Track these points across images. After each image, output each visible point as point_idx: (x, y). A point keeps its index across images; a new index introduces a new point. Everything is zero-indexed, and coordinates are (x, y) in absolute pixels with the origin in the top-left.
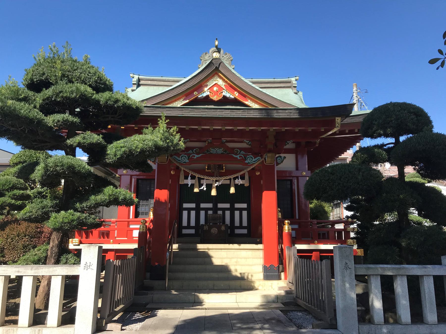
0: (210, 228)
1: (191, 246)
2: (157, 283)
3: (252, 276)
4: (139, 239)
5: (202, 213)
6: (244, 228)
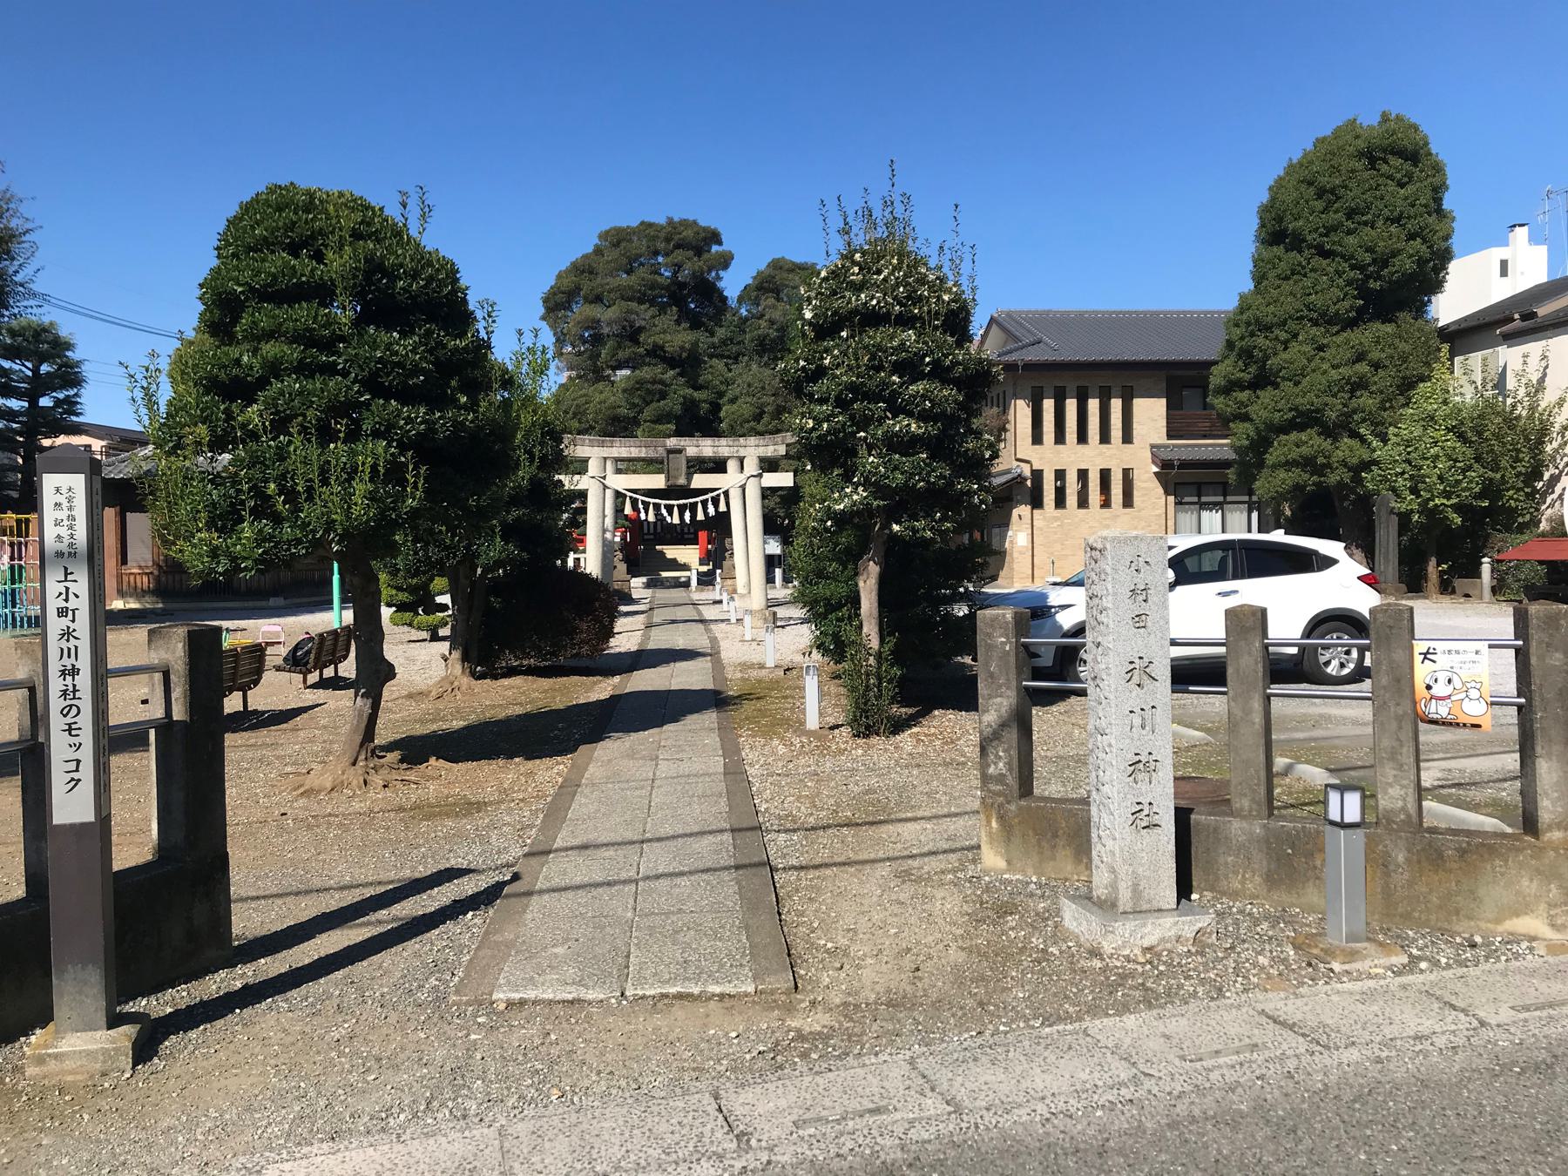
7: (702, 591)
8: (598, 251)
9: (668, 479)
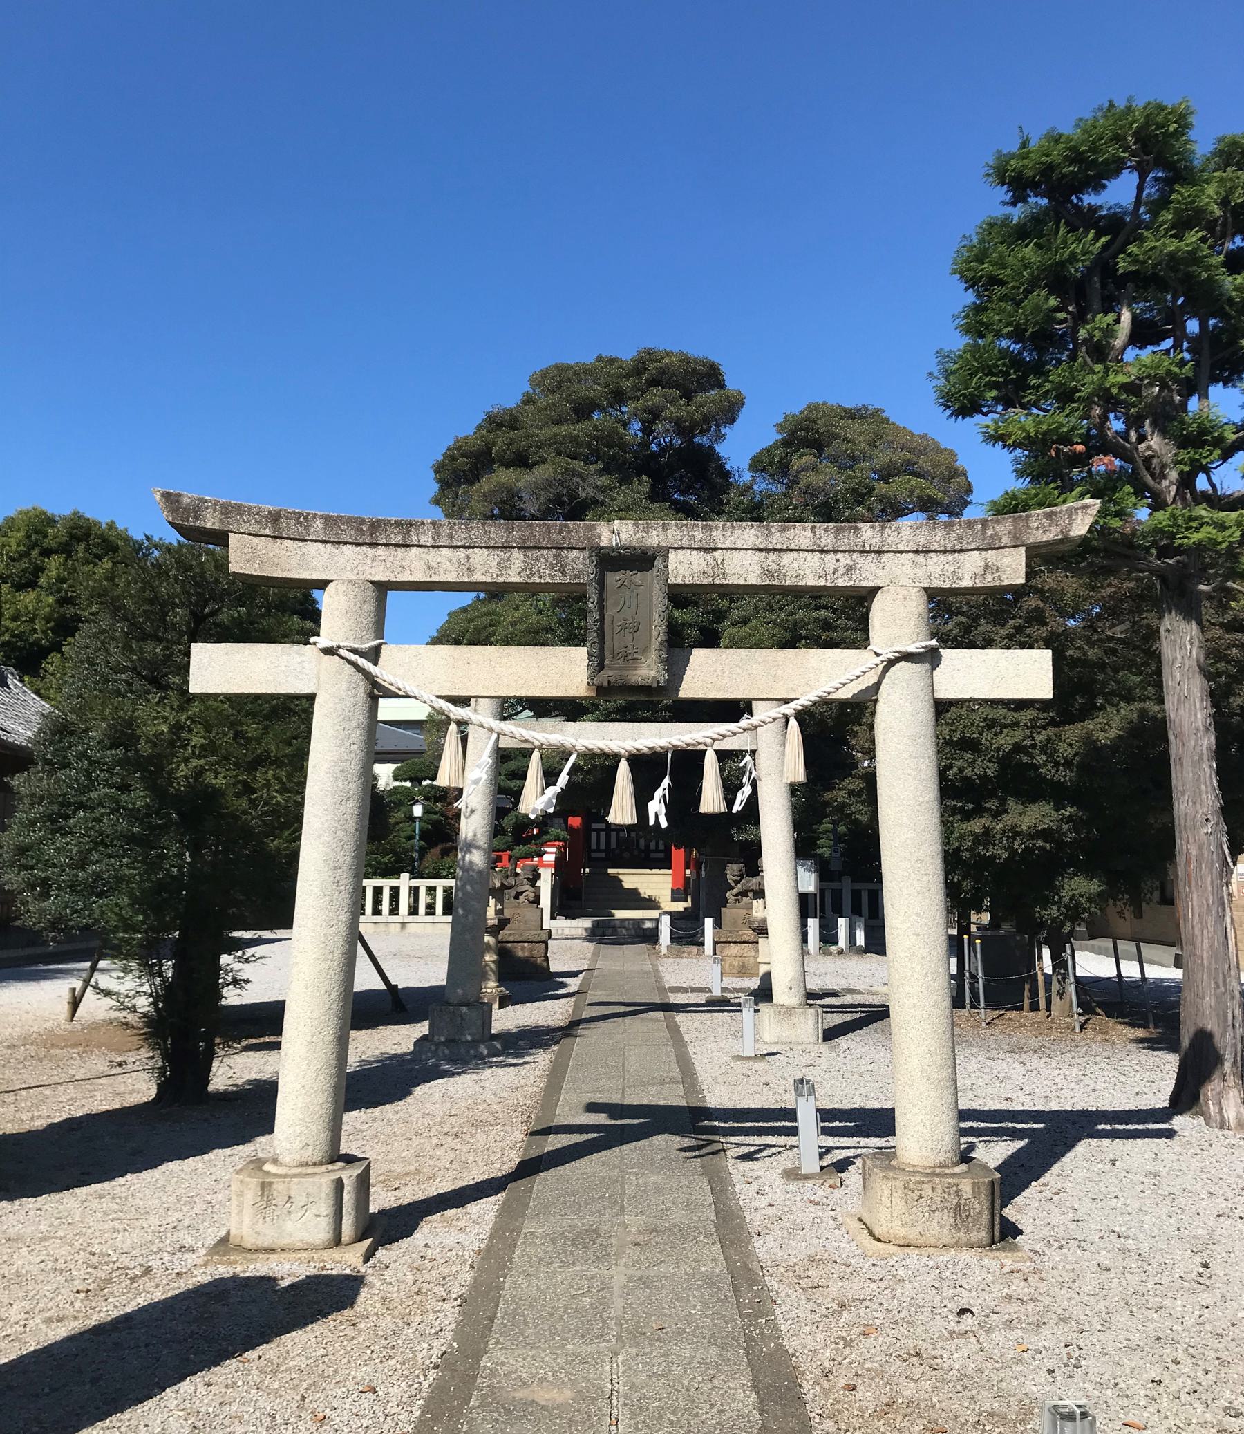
7: (679, 955)
8: (528, 401)
9: (598, 663)
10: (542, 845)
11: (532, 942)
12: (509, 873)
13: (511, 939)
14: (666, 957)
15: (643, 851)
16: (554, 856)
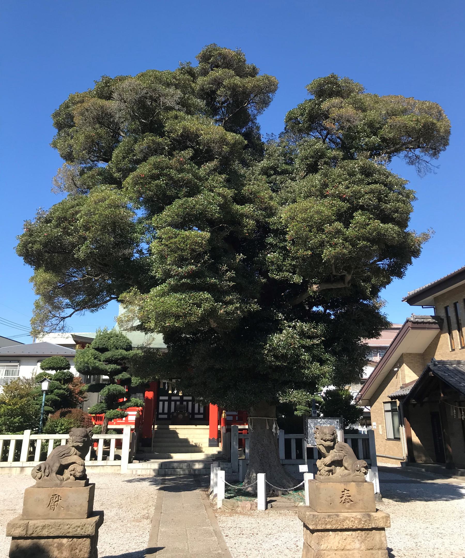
0: (178, 414)
1: (165, 426)
2: (146, 449)
3: (202, 445)
4: (135, 422)
5: (173, 403)
6: (201, 414)
7: (233, 511)
10: (126, 409)
11: (73, 537)
12: (102, 429)
13: (45, 533)
14: (223, 512)
15: (190, 414)
16: (135, 417)
